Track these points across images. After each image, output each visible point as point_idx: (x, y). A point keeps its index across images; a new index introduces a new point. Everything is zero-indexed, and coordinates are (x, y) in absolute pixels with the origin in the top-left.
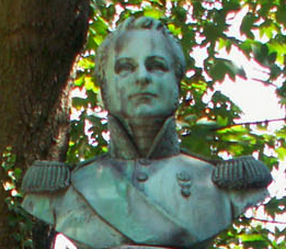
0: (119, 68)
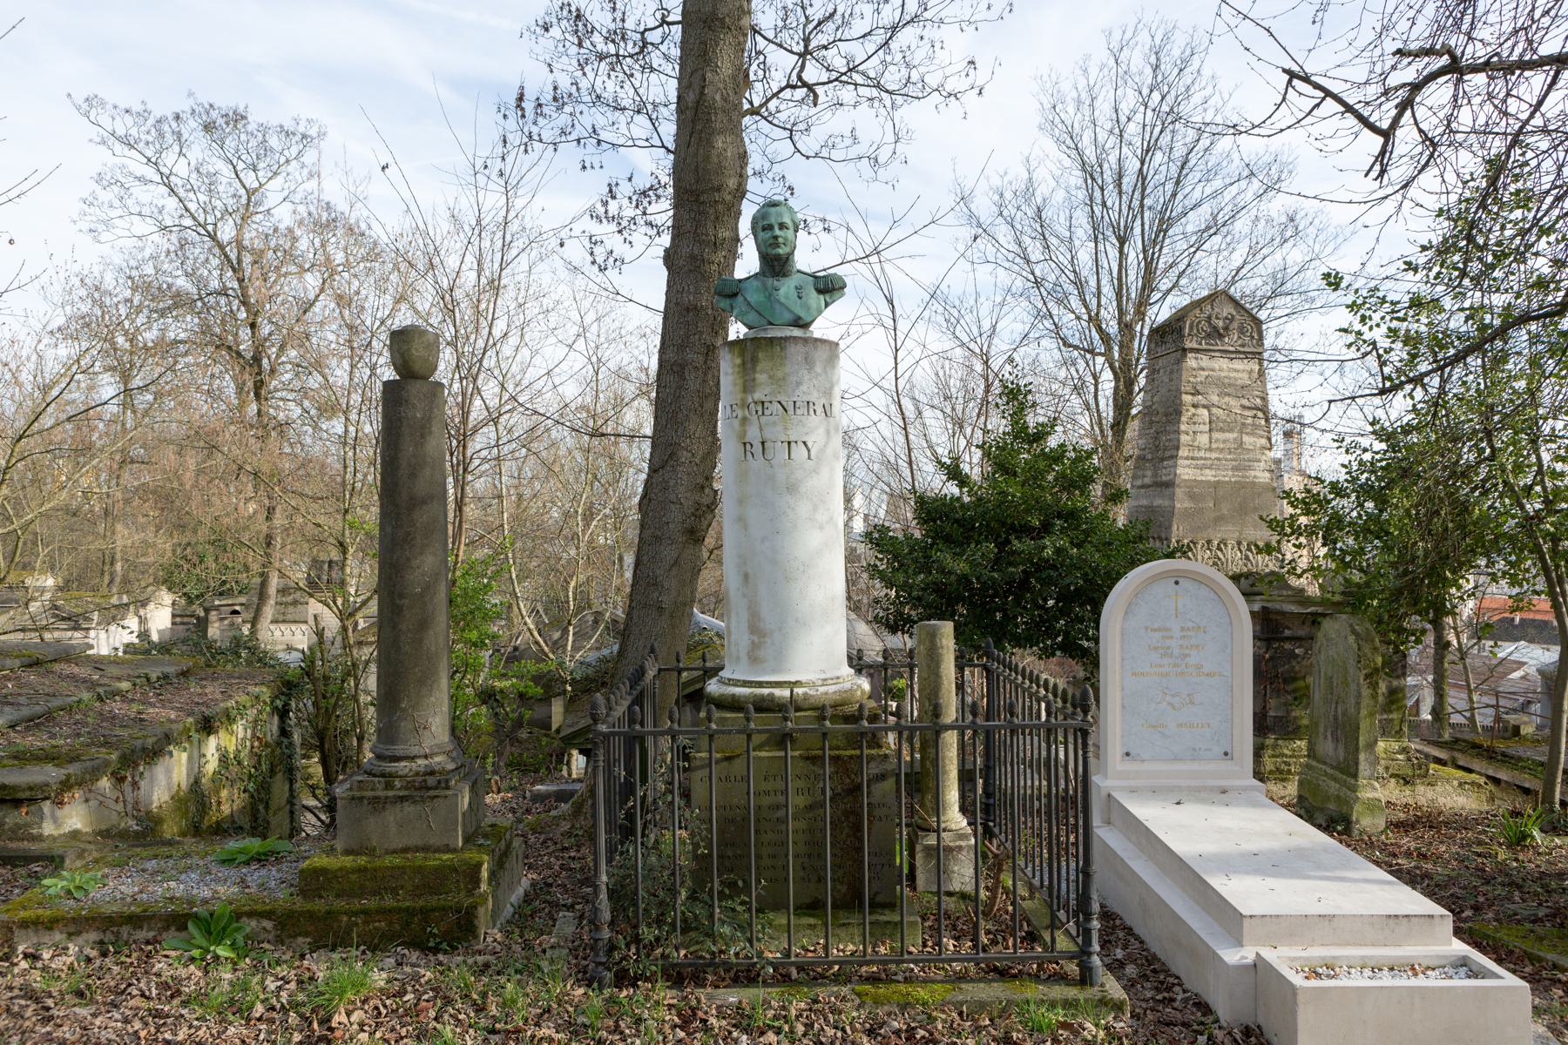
0: (764, 229)
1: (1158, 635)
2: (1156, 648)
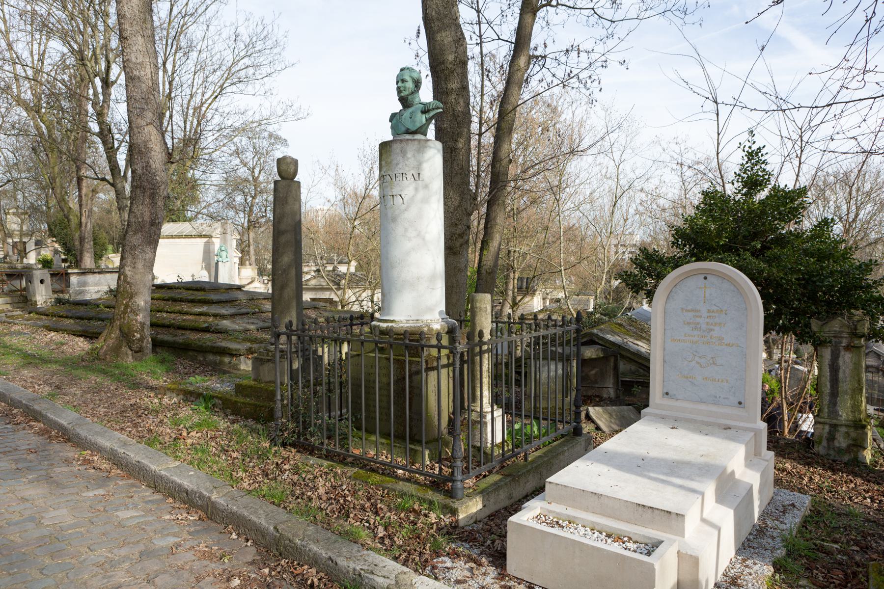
1: (690, 314)
2: (689, 324)
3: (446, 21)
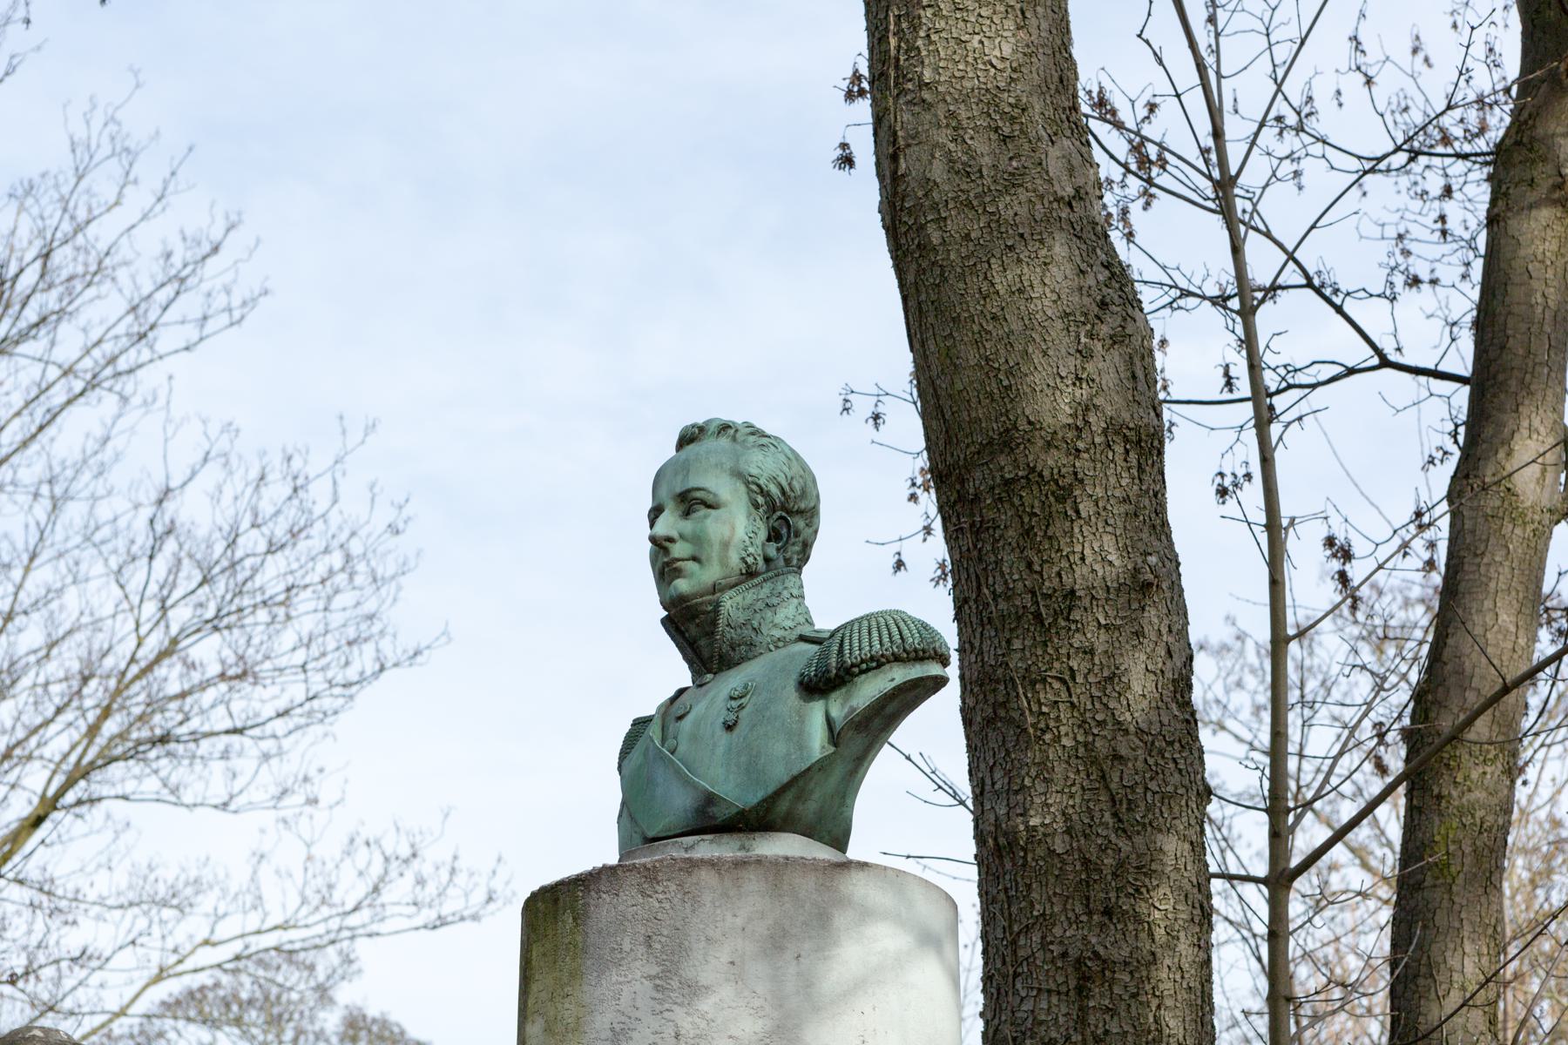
3: (1013, 206)
